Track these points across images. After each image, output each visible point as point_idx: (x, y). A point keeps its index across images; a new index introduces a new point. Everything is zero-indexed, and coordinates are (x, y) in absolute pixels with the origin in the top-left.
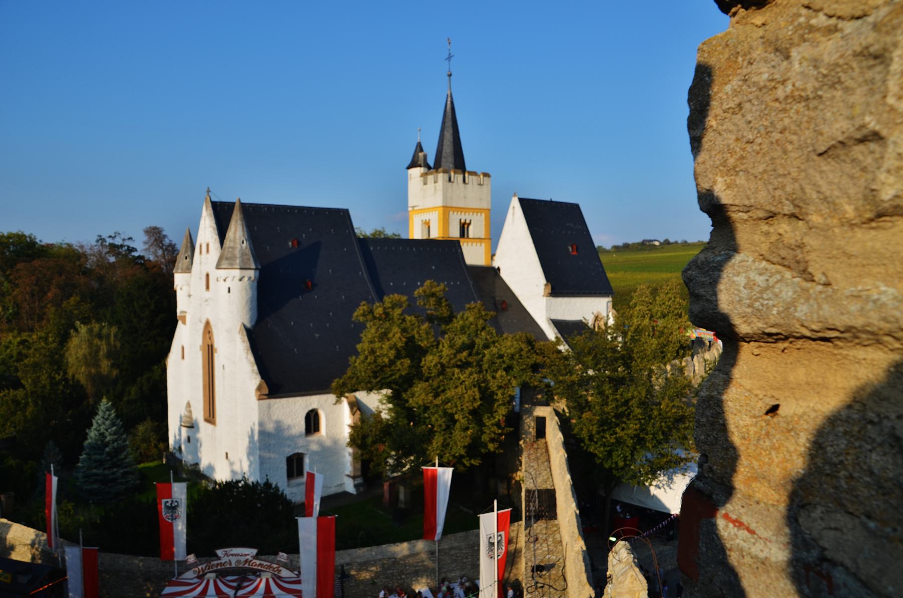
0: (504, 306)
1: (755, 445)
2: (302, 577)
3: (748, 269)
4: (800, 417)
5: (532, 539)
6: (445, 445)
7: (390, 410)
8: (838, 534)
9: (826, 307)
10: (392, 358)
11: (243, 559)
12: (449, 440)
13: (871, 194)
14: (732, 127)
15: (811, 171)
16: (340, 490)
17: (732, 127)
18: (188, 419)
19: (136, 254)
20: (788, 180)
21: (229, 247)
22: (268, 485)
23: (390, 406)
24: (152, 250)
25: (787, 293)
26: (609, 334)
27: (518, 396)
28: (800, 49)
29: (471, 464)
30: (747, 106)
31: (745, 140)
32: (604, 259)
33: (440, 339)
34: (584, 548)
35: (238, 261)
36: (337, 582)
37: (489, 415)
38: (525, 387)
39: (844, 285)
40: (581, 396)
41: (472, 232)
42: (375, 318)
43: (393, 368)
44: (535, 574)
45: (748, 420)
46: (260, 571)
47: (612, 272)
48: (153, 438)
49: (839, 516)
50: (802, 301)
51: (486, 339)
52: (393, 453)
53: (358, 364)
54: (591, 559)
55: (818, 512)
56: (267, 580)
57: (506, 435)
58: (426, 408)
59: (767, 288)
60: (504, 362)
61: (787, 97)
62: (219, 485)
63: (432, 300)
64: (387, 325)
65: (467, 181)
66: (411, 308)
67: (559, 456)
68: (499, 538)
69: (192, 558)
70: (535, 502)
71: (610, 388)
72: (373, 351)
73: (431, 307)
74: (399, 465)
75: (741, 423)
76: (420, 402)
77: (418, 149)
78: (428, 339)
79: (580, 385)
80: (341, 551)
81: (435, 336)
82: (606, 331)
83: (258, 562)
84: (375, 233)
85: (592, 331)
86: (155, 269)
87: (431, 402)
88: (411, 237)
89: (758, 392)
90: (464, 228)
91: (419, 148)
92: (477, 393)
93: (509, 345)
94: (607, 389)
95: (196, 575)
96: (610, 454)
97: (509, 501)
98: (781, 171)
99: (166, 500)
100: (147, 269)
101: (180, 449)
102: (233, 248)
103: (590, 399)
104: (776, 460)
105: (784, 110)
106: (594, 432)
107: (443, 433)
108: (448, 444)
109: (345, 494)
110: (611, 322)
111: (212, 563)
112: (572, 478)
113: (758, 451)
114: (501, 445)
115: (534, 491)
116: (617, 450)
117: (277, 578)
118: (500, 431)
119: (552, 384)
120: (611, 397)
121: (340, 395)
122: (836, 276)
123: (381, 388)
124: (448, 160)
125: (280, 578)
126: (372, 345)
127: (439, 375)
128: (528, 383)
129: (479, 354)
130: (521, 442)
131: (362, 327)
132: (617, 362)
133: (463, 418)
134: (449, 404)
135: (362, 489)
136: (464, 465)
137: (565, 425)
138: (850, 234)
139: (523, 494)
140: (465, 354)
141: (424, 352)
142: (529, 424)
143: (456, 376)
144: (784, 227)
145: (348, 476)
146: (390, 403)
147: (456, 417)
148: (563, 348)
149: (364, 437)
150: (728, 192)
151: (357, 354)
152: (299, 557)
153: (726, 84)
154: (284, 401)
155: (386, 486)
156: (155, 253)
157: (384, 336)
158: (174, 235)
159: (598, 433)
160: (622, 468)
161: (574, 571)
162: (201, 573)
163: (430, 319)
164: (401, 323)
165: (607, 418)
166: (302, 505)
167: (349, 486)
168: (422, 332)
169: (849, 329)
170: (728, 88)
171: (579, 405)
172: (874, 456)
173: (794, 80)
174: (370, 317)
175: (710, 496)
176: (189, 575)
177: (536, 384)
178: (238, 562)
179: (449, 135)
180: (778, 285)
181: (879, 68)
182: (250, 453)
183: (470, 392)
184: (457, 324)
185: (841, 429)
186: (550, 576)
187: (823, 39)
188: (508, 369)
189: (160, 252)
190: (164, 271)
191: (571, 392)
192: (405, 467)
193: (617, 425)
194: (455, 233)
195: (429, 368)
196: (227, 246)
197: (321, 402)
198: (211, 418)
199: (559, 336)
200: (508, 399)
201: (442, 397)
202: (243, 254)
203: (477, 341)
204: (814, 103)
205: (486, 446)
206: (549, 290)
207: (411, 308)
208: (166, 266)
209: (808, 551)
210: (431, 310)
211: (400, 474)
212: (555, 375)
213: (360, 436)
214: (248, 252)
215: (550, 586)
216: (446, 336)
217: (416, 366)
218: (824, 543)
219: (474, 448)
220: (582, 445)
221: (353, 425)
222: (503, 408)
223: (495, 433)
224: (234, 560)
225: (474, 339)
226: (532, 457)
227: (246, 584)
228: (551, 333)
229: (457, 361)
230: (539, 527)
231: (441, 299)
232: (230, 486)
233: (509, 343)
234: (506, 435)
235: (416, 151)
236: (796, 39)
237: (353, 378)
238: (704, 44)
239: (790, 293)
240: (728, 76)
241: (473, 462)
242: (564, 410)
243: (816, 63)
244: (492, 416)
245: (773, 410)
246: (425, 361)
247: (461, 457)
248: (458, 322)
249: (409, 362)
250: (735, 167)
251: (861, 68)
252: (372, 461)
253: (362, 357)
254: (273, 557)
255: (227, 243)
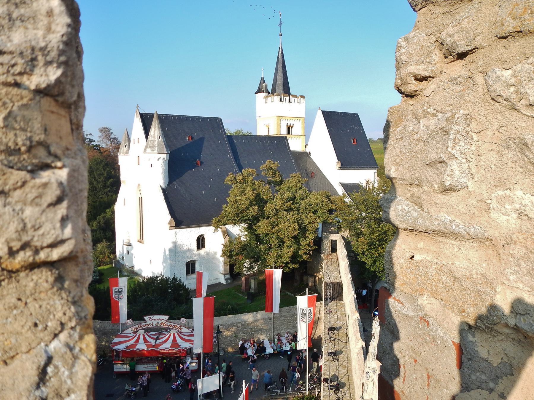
0: (313, 175)
1: (405, 271)
2: (194, 333)
3: (402, 204)
4: (421, 261)
5: (328, 312)
6: (278, 256)
7: (246, 235)
8: (432, 306)
9: (427, 222)
10: (247, 205)
11: (160, 322)
12: (280, 253)
13: (443, 183)
14: (399, 146)
15: (424, 170)
16: (216, 282)
17: (399, 146)
18: (128, 241)
19: (94, 144)
20: (416, 172)
21: (151, 140)
22: (175, 279)
23: (246, 233)
24: (104, 141)
25: (415, 215)
26: (375, 192)
27: (321, 228)
28: (424, 120)
29: (292, 267)
30: (404, 139)
31: (403, 152)
32: (372, 146)
33: (275, 194)
34: (359, 318)
35: (156, 149)
36: (215, 336)
37: (304, 239)
38: (324, 223)
39: (434, 215)
40: (358, 228)
41: (294, 131)
42: (237, 182)
43: (248, 211)
44: (330, 332)
45: (403, 261)
46: (170, 329)
47: (378, 154)
48: (107, 251)
49: (432, 299)
50: (420, 218)
51: (302, 195)
52: (248, 260)
53: (228, 209)
54: (363, 325)
55: (424, 298)
56: (174, 334)
57: (313, 250)
58: (267, 235)
59: (409, 212)
60: (312, 208)
61: (417, 139)
62: (147, 279)
63: (271, 172)
64: (244, 186)
65: (291, 101)
66: (258, 177)
67: (344, 263)
68: (309, 311)
69: (130, 322)
70: (330, 290)
71: (375, 224)
72: (236, 202)
73: (270, 176)
74: (251, 268)
75: (400, 262)
76: (264, 232)
77: (262, 81)
78: (268, 194)
79: (357, 222)
80: (217, 317)
81: (272, 193)
82: (373, 190)
83: (169, 324)
84: (237, 132)
85: (365, 191)
86: (107, 152)
87: (270, 231)
88: (258, 135)
89: (407, 250)
90: (289, 129)
91: (263, 81)
92: (296, 226)
93: (315, 198)
94: (373, 224)
95: (132, 332)
96: (375, 262)
97: (315, 290)
98: (414, 168)
99: (115, 288)
100: (101, 153)
101: (123, 258)
102: (154, 141)
103: (363, 230)
104: (412, 277)
105: (416, 144)
106: (365, 250)
107: (277, 249)
108: (280, 256)
109: (220, 284)
110: (376, 185)
111: (142, 324)
112: (352, 276)
113: (406, 274)
114: (311, 256)
115: (330, 284)
116: (379, 261)
117: (180, 333)
118: (310, 248)
119: (341, 221)
120: (376, 229)
121: (217, 227)
122: (431, 210)
123: (241, 223)
124: (280, 88)
125: (181, 333)
126: (236, 198)
127: (274, 216)
128: (326, 221)
129: (298, 203)
130: (322, 255)
131: (229, 187)
132: (379, 208)
133: (288, 241)
134: (281, 232)
135: (229, 281)
136: (289, 268)
137: (348, 245)
138: (436, 195)
139: (323, 285)
140: (290, 203)
141: (266, 202)
142: (327, 245)
143: (284, 216)
144: (415, 189)
145: (222, 274)
146: (246, 231)
147: (284, 240)
148: (348, 200)
149: (231, 251)
150: (396, 173)
151: (227, 203)
152: (193, 321)
153: (398, 127)
154: (184, 230)
155: (243, 279)
156: (106, 143)
157: (243, 193)
158: (118, 132)
159: (368, 250)
160: (382, 271)
161: (353, 331)
162: (135, 330)
163: (269, 183)
164: (252, 185)
165: (373, 241)
166: (195, 291)
167: (223, 280)
168: (265, 191)
169: (434, 231)
170: (398, 129)
171: (357, 233)
172: (444, 278)
173: (420, 133)
174: (234, 181)
175: (389, 290)
176: (129, 331)
177: (331, 221)
178: (157, 323)
179: (280, 73)
180: (412, 211)
181: (447, 136)
182: (165, 261)
183: (293, 226)
184: (285, 186)
185: (434, 267)
186: (338, 334)
187: (432, 118)
188: (315, 212)
189: (109, 142)
190: (112, 154)
191: (352, 225)
192: (254, 269)
193: (379, 246)
194: (284, 132)
195: (269, 212)
196: (150, 139)
197: (207, 231)
198: (141, 240)
199: (345, 193)
200: (315, 229)
201: (277, 228)
202: (159, 144)
203: (297, 196)
204: (426, 144)
205: (302, 257)
206: (339, 165)
207: (258, 177)
208: (113, 151)
209: (421, 312)
210: (270, 177)
211: (251, 272)
212: (342, 216)
213: (229, 251)
214: (163, 143)
215: (339, 340)
216: (279, 193)
217: (261, 210)
218: (427, 309)
219: (294, 258)
220: (358, 257)
221: (224, 244)
222: (312, 235)
223: (307, 250)
224: (155, 322)
225: (295, 194)
226: (329, 264)
227: (161, 336)
228: (340, 191)
229: (285, 207)
230: (332, 305)
231: (276, 171)
232: (152, 280)
233: (315, 197)
234: (313, 250)
235: (261, 82)
236: (423, 116)
237: (225, 217)
238: (391, 108)
239: (416, 215)
240: (399, 124)
241: (294, 266)
242: (347, 237)
243: (428, 128)
244: (305, 239)
245: (413, 257)
246: (266, 207)
247: (287, 263)
248: (286, 184)
249: (257, 208)
250: (399, 163)
251: (442, 134)
252: (236, 265)
253: (230, 205)
254: (178, 320)
255: (150, 138)
